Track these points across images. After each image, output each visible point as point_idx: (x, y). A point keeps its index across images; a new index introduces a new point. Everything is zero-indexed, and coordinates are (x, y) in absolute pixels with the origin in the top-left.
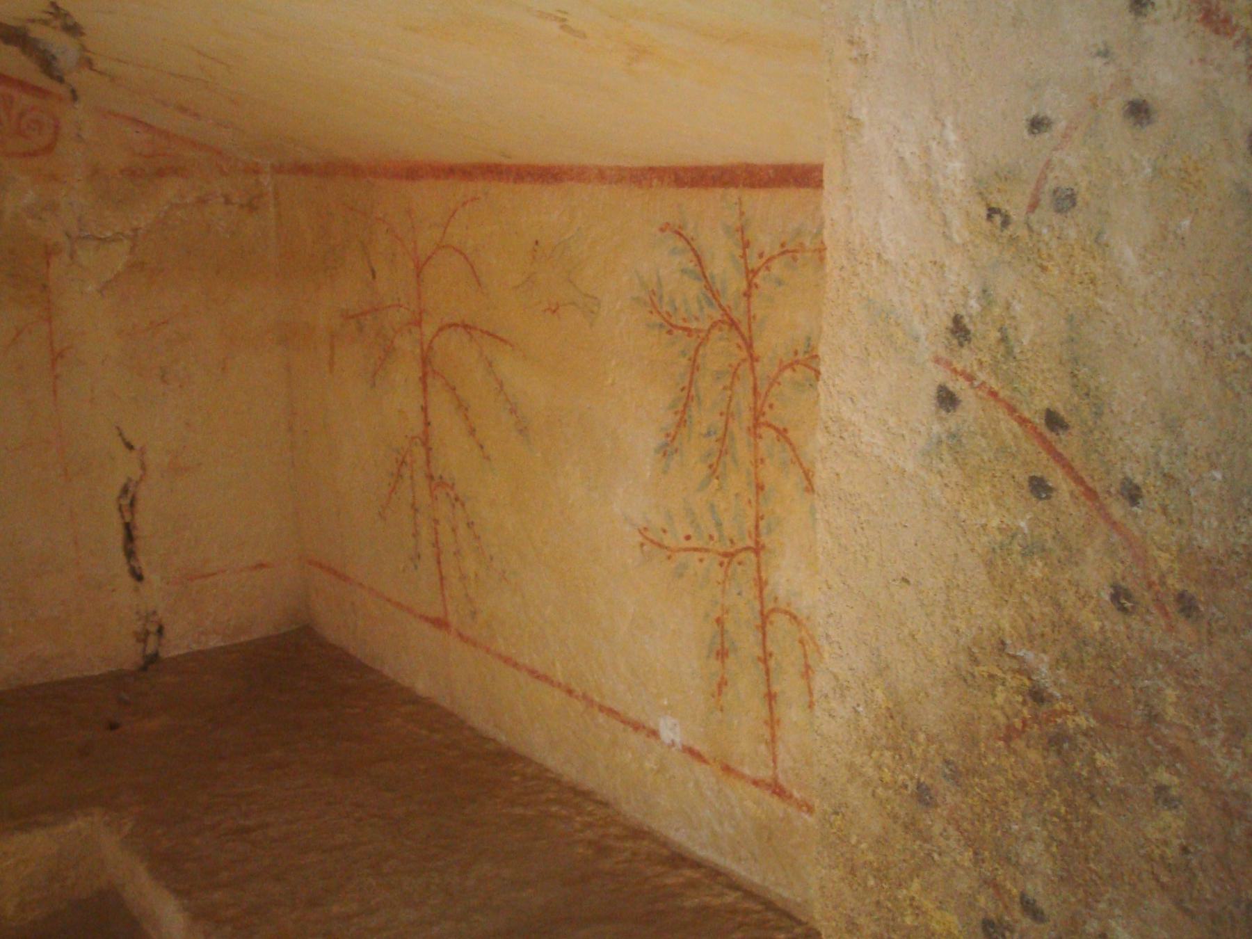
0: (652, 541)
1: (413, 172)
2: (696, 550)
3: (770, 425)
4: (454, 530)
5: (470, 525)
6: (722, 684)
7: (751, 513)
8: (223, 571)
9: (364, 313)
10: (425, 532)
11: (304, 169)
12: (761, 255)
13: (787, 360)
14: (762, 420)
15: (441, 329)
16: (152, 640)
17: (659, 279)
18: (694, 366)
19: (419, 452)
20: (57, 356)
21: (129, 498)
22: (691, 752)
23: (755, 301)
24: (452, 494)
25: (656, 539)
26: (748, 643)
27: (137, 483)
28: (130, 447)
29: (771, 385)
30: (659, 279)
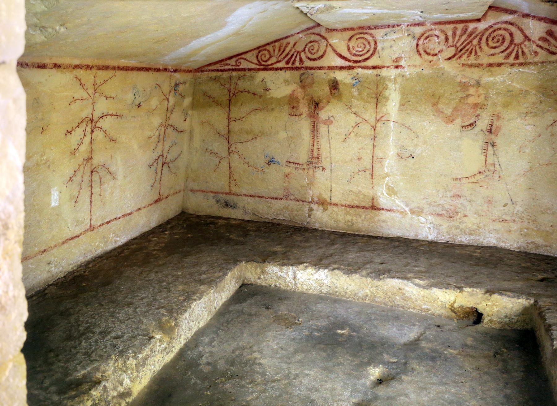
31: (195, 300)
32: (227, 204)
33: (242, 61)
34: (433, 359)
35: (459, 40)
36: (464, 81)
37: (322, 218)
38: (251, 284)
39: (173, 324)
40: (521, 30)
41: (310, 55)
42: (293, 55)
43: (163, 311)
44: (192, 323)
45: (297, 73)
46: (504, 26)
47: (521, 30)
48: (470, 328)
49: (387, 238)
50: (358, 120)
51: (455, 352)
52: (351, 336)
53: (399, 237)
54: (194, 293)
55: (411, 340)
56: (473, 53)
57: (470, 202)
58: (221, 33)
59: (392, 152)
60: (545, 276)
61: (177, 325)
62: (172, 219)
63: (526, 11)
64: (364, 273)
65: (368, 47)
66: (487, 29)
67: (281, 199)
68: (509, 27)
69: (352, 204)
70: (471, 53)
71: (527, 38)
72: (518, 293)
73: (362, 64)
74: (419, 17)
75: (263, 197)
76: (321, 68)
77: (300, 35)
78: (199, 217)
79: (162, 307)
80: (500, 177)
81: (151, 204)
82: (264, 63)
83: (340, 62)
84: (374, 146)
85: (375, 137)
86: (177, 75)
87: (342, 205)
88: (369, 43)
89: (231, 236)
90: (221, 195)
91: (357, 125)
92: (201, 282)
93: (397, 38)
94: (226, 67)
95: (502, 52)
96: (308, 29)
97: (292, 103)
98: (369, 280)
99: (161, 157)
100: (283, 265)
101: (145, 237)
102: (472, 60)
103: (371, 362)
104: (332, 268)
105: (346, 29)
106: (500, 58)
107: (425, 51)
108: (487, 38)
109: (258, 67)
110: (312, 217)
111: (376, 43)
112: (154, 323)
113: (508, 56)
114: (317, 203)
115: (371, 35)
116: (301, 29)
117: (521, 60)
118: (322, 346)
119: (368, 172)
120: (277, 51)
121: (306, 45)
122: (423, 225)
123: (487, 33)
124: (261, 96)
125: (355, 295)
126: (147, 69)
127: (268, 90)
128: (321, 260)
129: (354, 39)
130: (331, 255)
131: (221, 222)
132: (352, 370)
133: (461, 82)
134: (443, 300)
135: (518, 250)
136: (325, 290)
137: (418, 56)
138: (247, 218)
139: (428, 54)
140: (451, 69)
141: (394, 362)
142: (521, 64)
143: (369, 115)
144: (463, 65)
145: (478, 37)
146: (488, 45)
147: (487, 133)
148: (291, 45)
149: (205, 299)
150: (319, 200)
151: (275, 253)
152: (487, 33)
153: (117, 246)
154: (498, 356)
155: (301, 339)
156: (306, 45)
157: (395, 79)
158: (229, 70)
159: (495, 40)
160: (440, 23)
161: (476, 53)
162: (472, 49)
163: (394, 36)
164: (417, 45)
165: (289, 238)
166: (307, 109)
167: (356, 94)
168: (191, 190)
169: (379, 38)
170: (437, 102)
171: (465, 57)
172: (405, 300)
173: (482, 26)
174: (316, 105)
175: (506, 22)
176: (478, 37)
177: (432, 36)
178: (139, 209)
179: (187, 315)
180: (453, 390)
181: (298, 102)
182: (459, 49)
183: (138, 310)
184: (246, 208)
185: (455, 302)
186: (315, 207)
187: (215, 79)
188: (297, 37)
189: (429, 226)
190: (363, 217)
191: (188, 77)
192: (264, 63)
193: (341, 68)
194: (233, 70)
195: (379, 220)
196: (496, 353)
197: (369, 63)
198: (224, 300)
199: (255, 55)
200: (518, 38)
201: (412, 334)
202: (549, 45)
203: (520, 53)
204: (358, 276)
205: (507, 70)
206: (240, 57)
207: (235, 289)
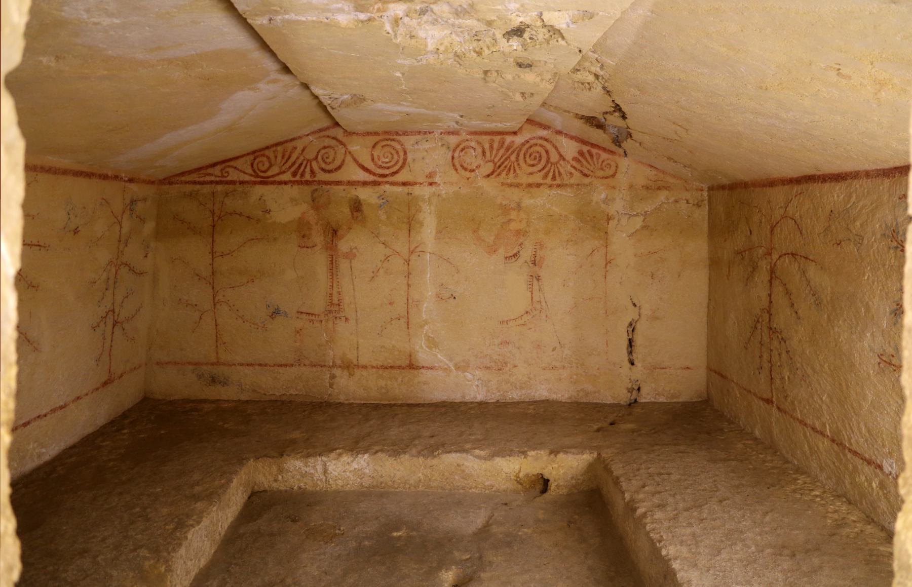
1: (772, 183)
5: (788, 352)
9: (745, 251)
10: (766, 356)
11: (723, 187)
15: (780, 257)
16: (635, 392)
17: (897, 224)
19: (766, 316)
20: (608, 262)
28: (635, 305)
30: (897, 224)
31: (192, 526)
32: (214, 380)
33: (230, 170)
34: (509, 545)
36: (504, 203)
37: (349, 387)
38: (265, 491)
39: (163, 569)
40: (556, 148)
41: (323, 166)
42: (301, 164)
43: (144, 552)
44: (189, 563)
45: (307, 189)
46: (540, 142)
47: (556, 148)
48: (538, 499)
49: (430, 405)
50: (388, 252)
51: (530, 531)
52: (411, 537)
53: (444, 402)
54: (188, 516)
56: (512, 171)
58: (209, 126)
59: (430, 292)
60: (600, 425)
61: (169, 569)
62: (129, 410)
63: (559, 128)
64: (414, 451)
65: (396, 157)
66: (523, 144)
67: (292, 365)
68: (545, 143)
69: (385, 364)
70: (509, 170)
71: (562, 157)
72: (581, 448)
73: (390, 179)
74: (454, 124)
75: (266, 365)
76: (338, 183)
77: (311, 138)
78: (172, 403)
79: (141, 547)
81: (97, 389)
82: (262, 174)
83: (362, 176)
84: (409, 285)
85: (409, 274)
86: (134, 187)
87: (373, 367)
88: (397, 152)
89: (226, 426)
90: (205, 368)
91: (387, 258)
92: (196, 498)
93: (430, 148)
94: (208, 178)
95: (540, 171)
96: (321, 130)
97: (302, 229)
98: (421, 459)
99: (111, 313)
100: (308, 456)
101: (89, 442)
103: (442, 565)
104: (374, 451)
105: (369, 134)
106: (538, 178)
107: (462, 166)
108: (525, 155)
109: (253, 179)
110: (335, 387)
111: (405, 153)
112: (131, 574)
113: (546, 176)
114: (340, 367)
115: (399, 142)
116: (312, 130)
118: (378, 558)
119: (403, 320)
120: (279, 158)
121: (318, 152)
124: (258, 220)
125: (405, 483)
126: (89, 175)
127: (268, 212)
128: (357, 442)
129: (379, 147)
130: (369, 434)
131: (207, 407)
132: (422, 580)
133: (501, 204)
134: (506, 470)
136: (367, 482)
137: (454, 172)
138: (244, 397)
139: (465, 169)
140: (490, 187)
141: (467, 559)
142: (559, 186)
143: (401, 246)
144: (503, 184)
148: (299, 150)
149: (205, 522)
150: (343, 362)
151: (293, 442)
153: (42, 462)
154: (572, 525)
155: (348, 555)
156: (318, 152)
157: (429, 199)
158: (212, 182)
159: (533, 157)
160: (475, 133)
163: (427, 146)
164: (453, 158)
165: (313, 419)
166: (322, 238)
167: (384, 217)
168: (158, 363)
169: (408, 147)
170: (478, 228)
172: (465, 479)
173: (519, 140)
174: (334, 232)
175: (541, 138)
178: (78, 398)
179: (182, 551)
181: (310, 229)
183: (99, 559)
184: (245, 382)
185: (520, 472)
186: (337, 372)
187: (191, 196)
188: (306, 140)
190: (400, 380)
191: (150, 191)
192: (262, 174)
193: (365, 184)
194: (217, 183)
195: (419, 382)
196: (569, 523)
197: (399, 178)
198: (230, 520)
199: (249, 163)
200: (554, 157)
201: (479, 520)
203: (557, 173)
204: (407, 456)
205: (546, 191)
206: (227, 164)
207: (243, 501)
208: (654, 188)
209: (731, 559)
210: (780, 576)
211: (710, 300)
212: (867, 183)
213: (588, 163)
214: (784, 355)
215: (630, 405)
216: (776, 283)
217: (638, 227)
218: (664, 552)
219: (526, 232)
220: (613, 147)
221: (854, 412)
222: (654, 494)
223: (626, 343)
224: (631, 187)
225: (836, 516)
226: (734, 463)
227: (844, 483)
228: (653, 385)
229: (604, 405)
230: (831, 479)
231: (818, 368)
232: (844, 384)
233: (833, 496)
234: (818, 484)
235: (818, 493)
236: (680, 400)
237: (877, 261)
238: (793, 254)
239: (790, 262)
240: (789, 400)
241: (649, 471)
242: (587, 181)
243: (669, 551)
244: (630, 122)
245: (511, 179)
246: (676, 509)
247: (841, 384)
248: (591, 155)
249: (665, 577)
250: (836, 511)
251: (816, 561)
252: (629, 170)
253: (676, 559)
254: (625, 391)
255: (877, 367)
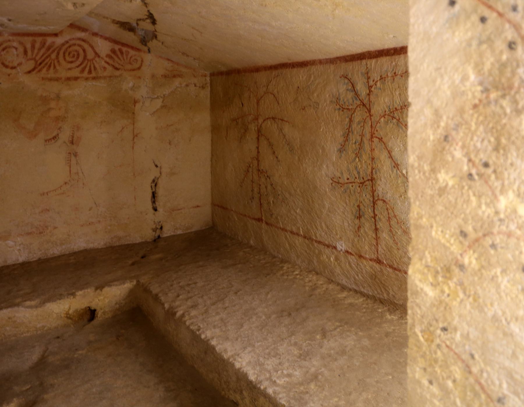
0: (335, 182)
1: (257, 69)
2: (350, 183)
3: (377, 137)
4: (266, 187)
5: (272, 185)
6: (359, 227)
7: (370, 167)
8: (184, 208)
9: (238, 119)
10: (256, 190)
11: (221, 73)
12: (373, 81)
13: (382, 114)
14: (374, 136)
15: (264, 120)
17: (339, 94)
18: (351, 120)
19: (255, 162)
20: (135, 136)
21: (155, 183)
22: (347, 252)
23: (371, 97)
24: (266, 175)
25: (337, 181)
26: (369, 212)
27: (158, 178)
28: (157, 166)
29: (377, 124)
30: (339, 94)
34: (67, 367)
35: (38, 53)
36: (44, 95)
40: (92, 47)
46: (78, 42)
47: (92, 47)
51: (84, 352)
55: (36, 361)
57: (58, 213)
63: (96, 30)
66: (63, 45)
68: (82, 43)
70: (50, 66)
71: (97, 55)
72: (122, 280)
80: (83, 184)
95: (78, 67)
102: (51, 74)
106: (76, 73)
108: (64, 53)
113: (83, 71)
117: (94, 74)
122: (12, 249)
123: (64, 48)
135: (105, 247)
139: (7, 67)
140: (30, 82)
142: (94, 78)
144: (43, 79)
145: (56, 52)
146: (65, 59)
147: (69, 144)
152: (64, 48)
159: (71, 55)
161: (55, 67)
162: (51, 63)
171: (44, 70)
172: (17, 327)
173: (59, 41)
175: (79, 39)
176: (56, 52)
177: (10, 47)
180: (98, 382)
182: (39, 62)
185: (69, 310)
189: (18, 248)
200: (90, 55)
202: (114, 61)
208: (171, 76)
209: (251, 328)
210: (284, 329)
211: (212, 155)
212: (320, 68)
213: (119, 59)
214: (269, 187)
215: (155, 241)
216: (262, 139)
217: (158, 106)
218: (203, 336)
219: (65, 117)
220: (140, 46)
221: (318, 217)
222: (187, 300)
223: (150, 195)
224: (153, 76)
225: (310, 284)
226: (239, 266)
227: (313, 262)
228: (172, 223)
229: (134, 245)
230: (304, 262)
231: (293, 192)
232: (310, 200)
233: (307, 272)
234: (297, 267)
235: (297, 273)
236: (193, 230)
237: (328, 118)
238: (273, 118)
239: (271, 123)
240: (274, 216)
241: (180, 284)
242: (117, 73)
243: (207, 334)
244: (158, 27)
245: (51, 74)
246: (205, 306)
247: (308, 201)
248: (122, 53)
249: (206, 353)
250: (310, 281)
251: (304, 314)
252: (152, 63)
253: (213, 338)
254: (151, 231)
255: (330, 186)
